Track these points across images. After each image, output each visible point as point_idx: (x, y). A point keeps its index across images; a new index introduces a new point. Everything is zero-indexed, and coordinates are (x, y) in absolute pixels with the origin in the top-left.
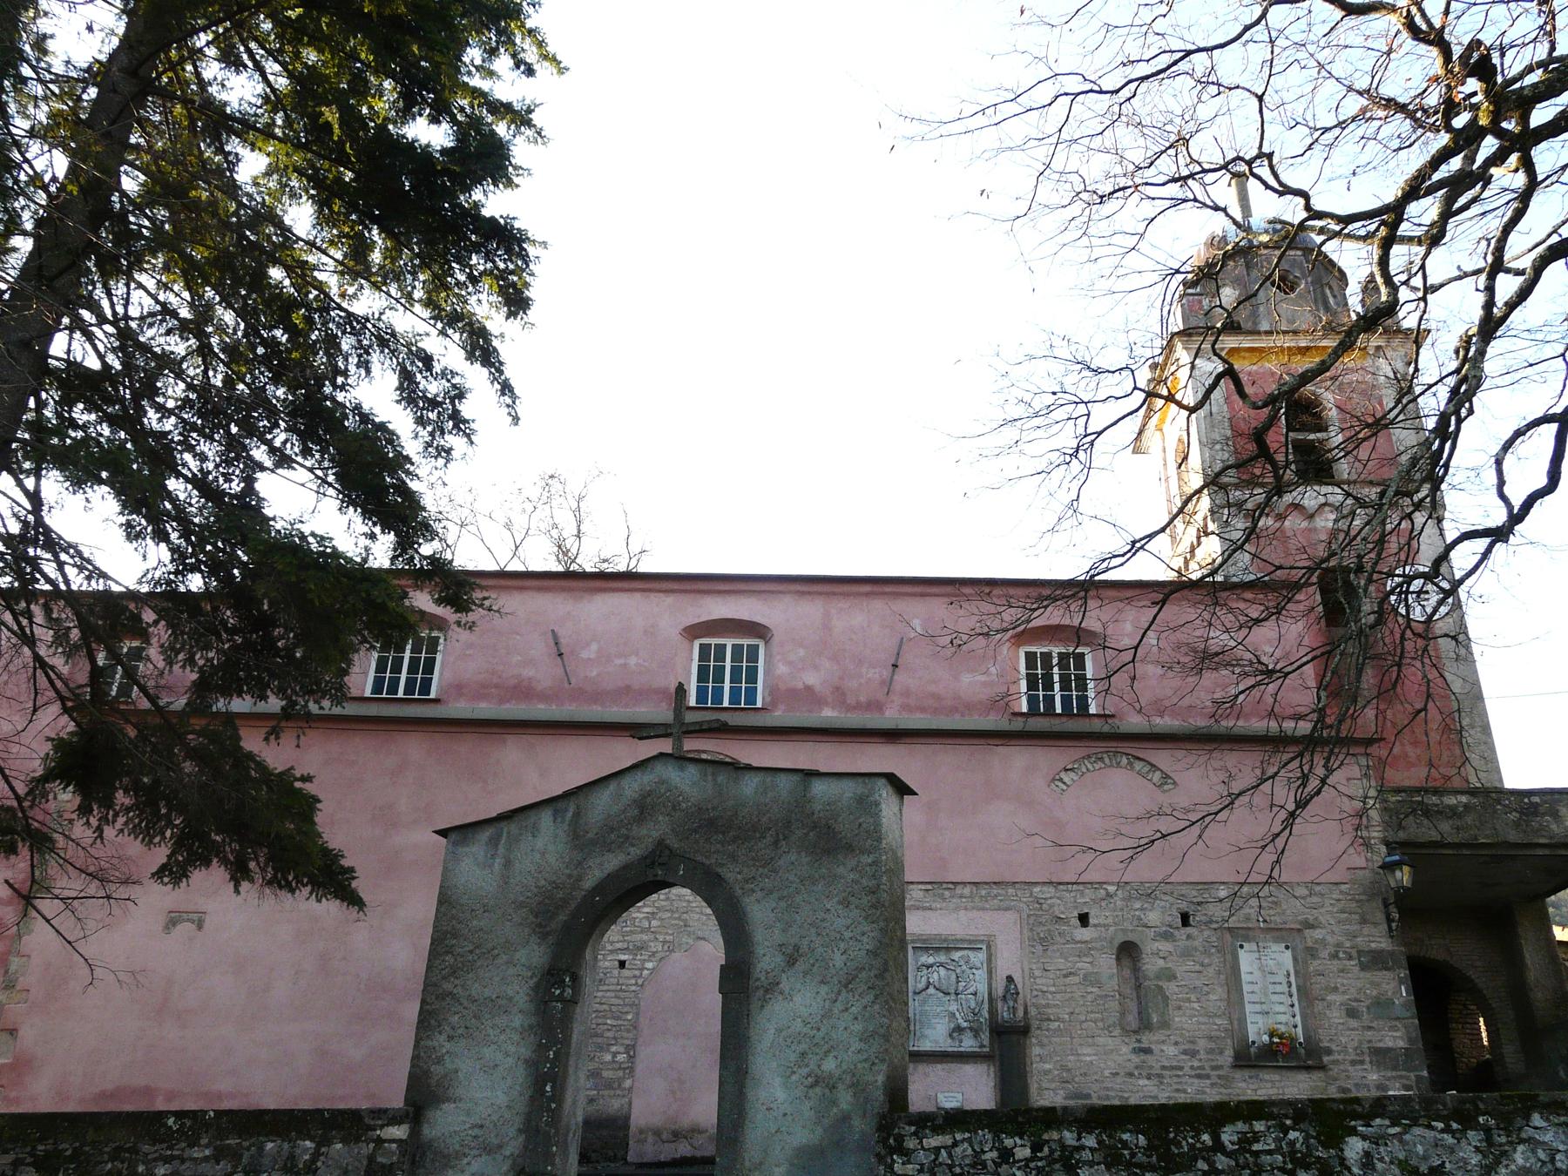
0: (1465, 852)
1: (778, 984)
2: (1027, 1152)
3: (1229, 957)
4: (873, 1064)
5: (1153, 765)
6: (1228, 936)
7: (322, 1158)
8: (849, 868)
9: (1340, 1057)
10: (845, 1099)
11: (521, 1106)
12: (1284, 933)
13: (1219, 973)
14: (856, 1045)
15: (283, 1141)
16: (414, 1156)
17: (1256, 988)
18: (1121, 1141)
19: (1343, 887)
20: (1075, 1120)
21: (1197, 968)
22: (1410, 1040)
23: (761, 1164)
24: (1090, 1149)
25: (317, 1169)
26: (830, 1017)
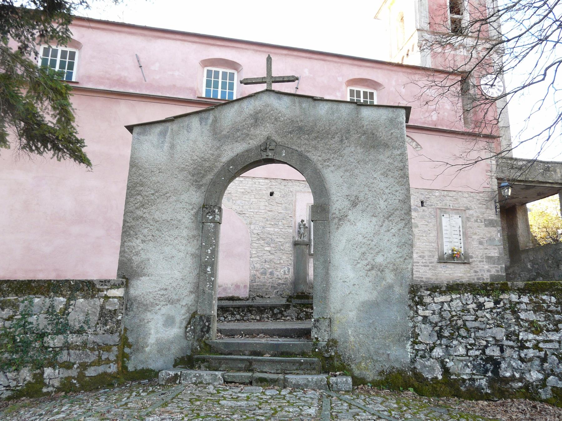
0: (522, 184)
1: (346, 216)
2: (492, 305)
3: (438, 220)
4: (405, 259)
5: (412, 139)
6: (438, 211)
7: (71, 307)
8: (387, 156)
9: (475, 260)
10: (390, 277)
11: (191, 278)
12: (459, 211)
14: (395, 249)
15: (46, 297)
16: (127, 304)
17: (448, 232)
18: (542, 299)
19: (481, 194)
20: (518, 289)
21: (426, 223)
22: (500, 254)
23: (341, 310)
24: (525, 303)
25: (69, 313)
26: (379, 234)
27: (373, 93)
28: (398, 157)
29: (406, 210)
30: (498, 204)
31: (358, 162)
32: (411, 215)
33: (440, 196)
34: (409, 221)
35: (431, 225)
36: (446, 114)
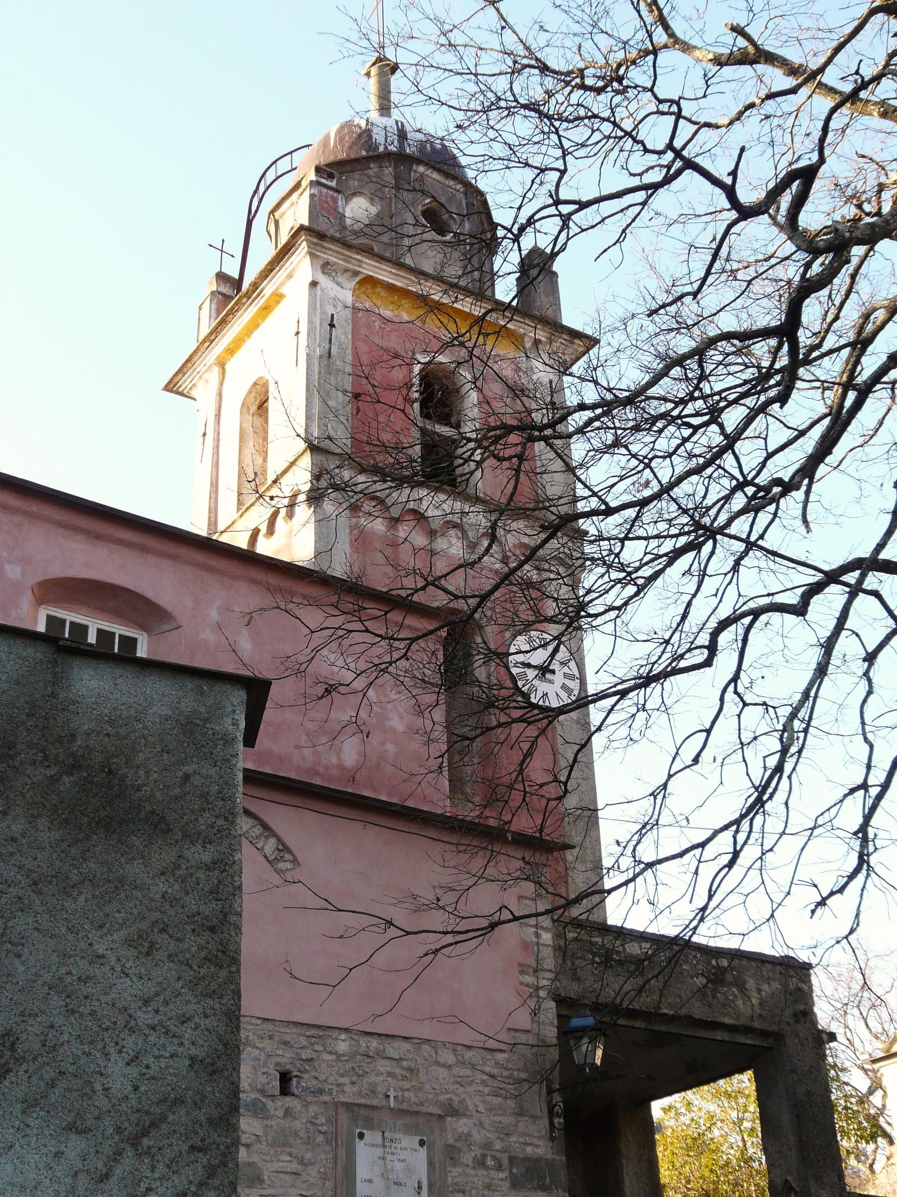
0: (638, 1024)
3: (342, 1152)
5: (266, 827)
6: (344, 1118)
13: (324, 1178)
19: (501, 1057)
21: (294, 1166)
27: (135, 640)
28: (200, 874)
29: (218, 1105)
30: (557, 1098)
31: (35, 883)
32: (235, 1128)
33: (353, 1056)
34: (228, 1155)
35: (313, 1173)
36: (390, 747)
